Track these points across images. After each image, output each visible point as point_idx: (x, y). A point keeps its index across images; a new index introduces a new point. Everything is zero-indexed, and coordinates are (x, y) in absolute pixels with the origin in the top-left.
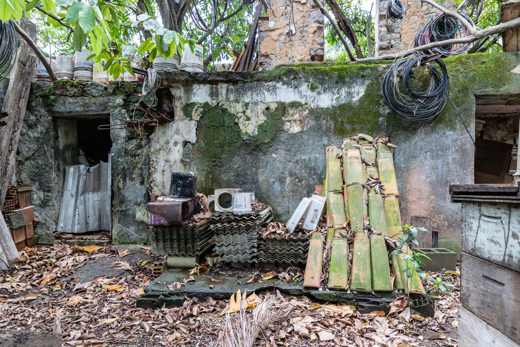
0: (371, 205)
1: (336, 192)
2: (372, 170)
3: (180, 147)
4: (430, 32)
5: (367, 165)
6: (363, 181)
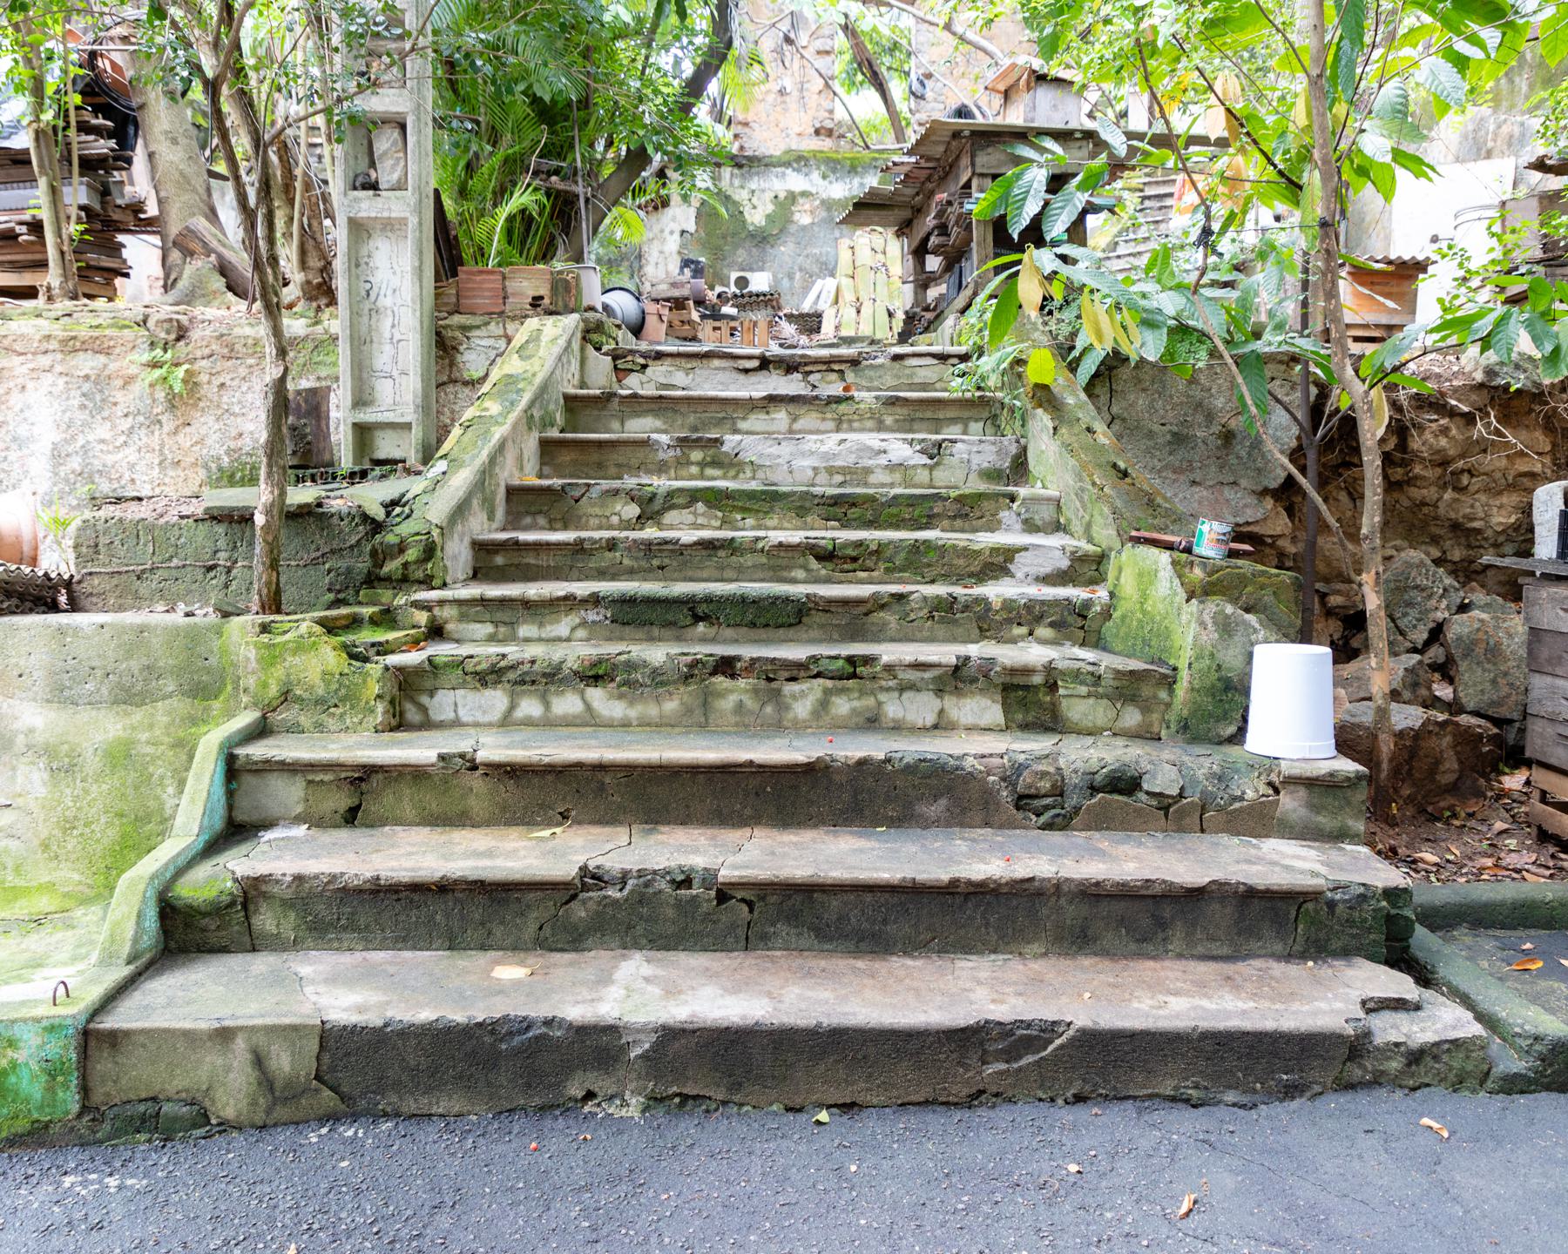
2: (880, 257)
3: (677, 236)
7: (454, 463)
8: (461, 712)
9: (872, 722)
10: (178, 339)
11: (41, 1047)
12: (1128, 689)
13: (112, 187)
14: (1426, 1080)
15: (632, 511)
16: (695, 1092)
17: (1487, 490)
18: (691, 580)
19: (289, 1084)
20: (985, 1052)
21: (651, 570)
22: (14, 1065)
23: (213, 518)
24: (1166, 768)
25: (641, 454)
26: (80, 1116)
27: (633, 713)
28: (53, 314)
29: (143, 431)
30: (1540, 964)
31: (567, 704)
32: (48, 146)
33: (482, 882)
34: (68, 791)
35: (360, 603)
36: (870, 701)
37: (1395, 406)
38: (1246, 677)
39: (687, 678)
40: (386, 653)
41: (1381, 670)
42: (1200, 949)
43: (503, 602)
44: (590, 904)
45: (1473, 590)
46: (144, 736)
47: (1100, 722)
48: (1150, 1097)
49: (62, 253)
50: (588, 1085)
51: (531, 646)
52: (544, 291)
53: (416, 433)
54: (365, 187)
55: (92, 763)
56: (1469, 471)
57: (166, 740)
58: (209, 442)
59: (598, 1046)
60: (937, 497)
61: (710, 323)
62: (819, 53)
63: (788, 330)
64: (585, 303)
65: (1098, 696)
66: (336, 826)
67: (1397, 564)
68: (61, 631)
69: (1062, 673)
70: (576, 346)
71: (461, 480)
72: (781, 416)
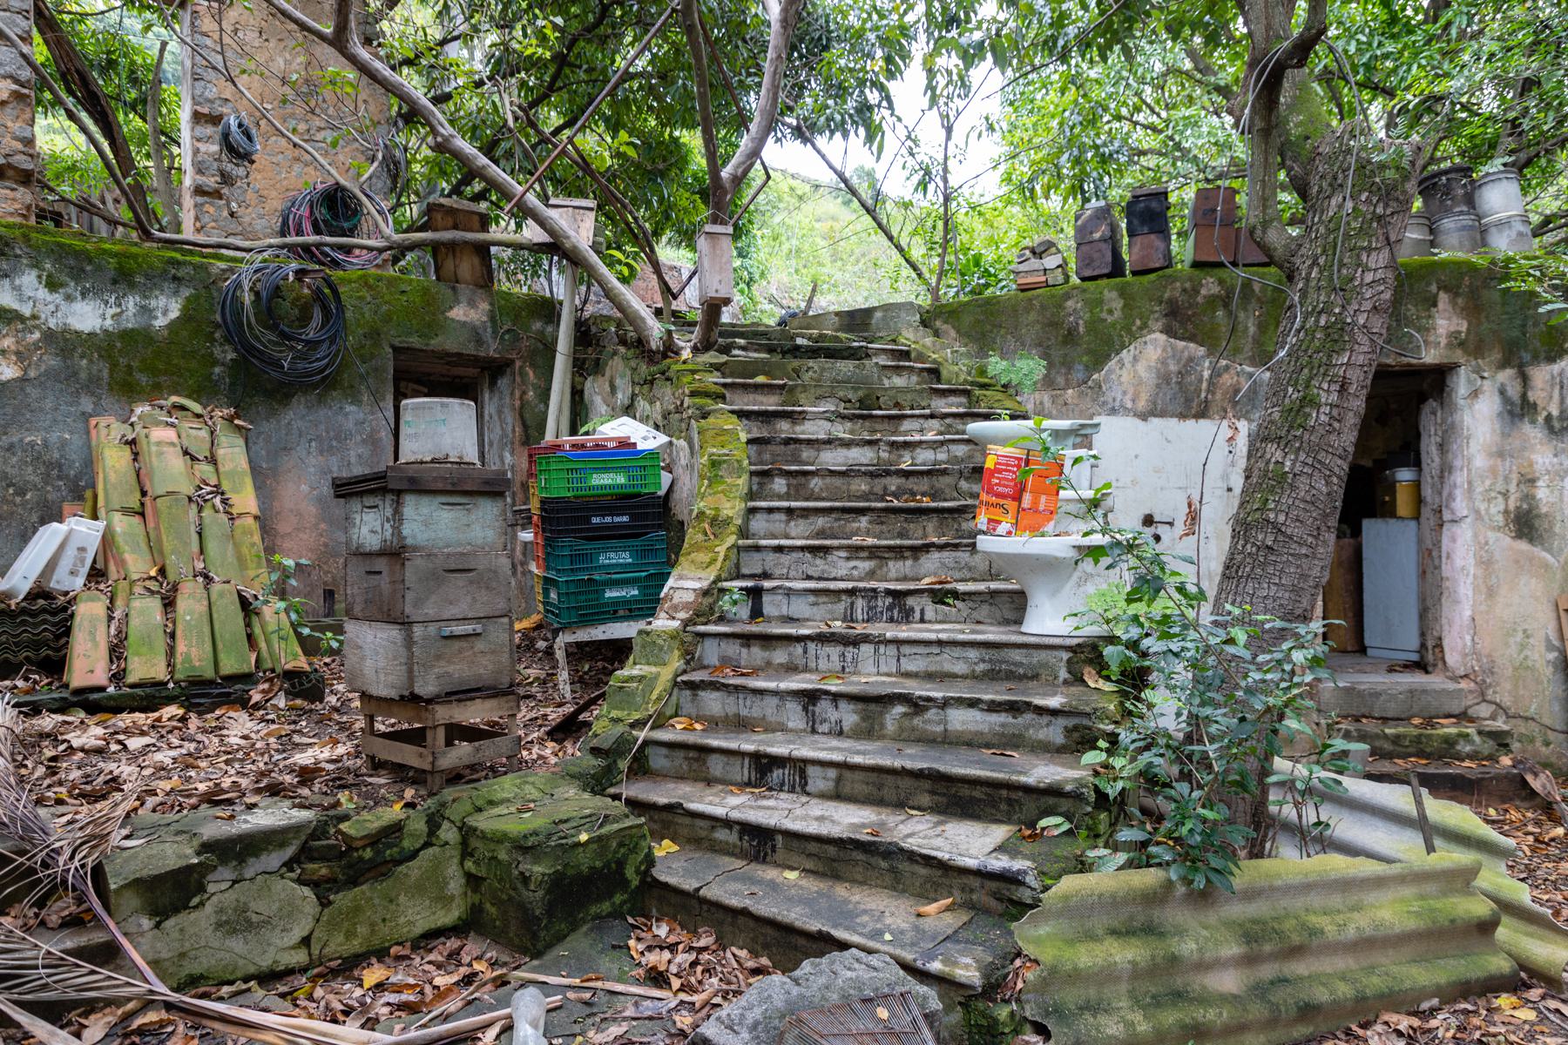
0: (207, 533)
1: (126, 511)
2: (205, 469)
4: (312, 212)
5: (193, 458)
6: (188, 489)
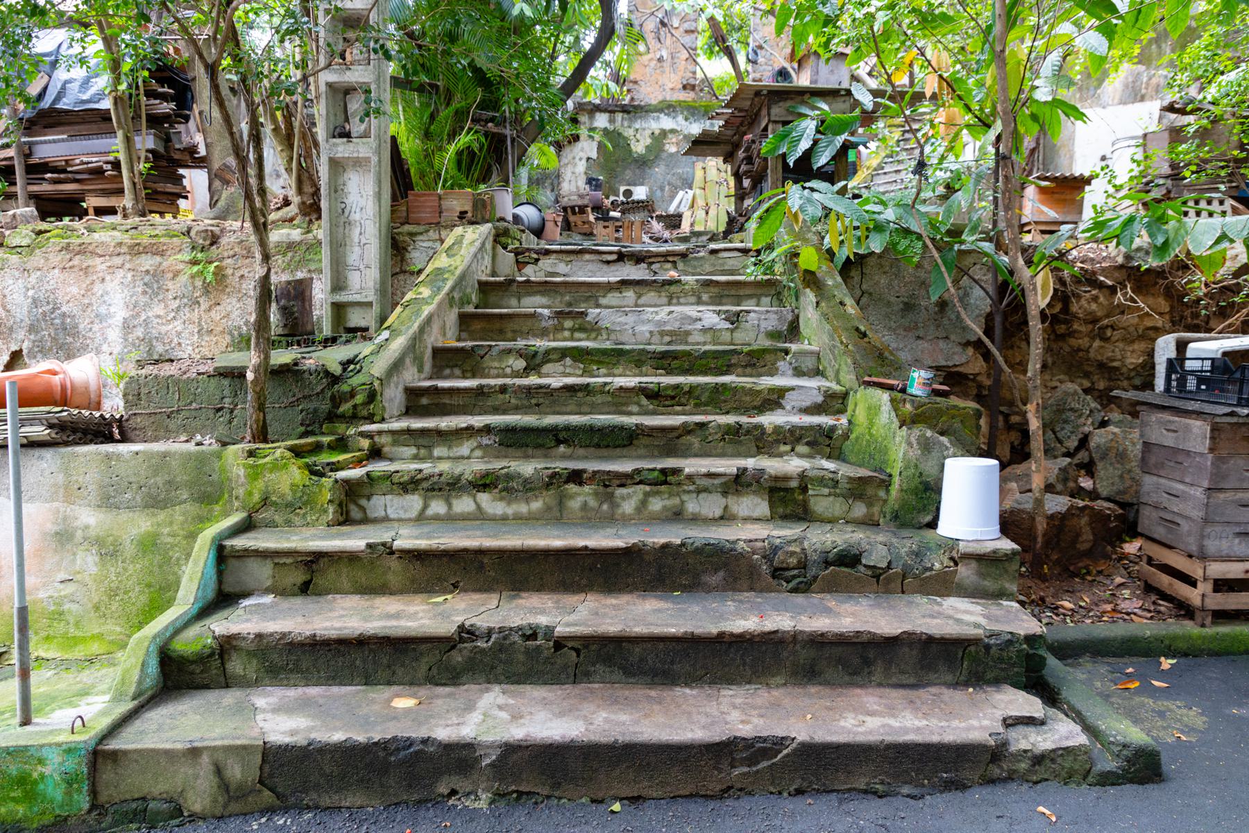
3: (584, 162)
7: (395, 333)
8: (389, 511)
9: (677, 516)
10: (212, 244)
11: (61, 764)
12: (858, 490)
13: (172, 136)
14: (1046, 776)
15: (520, 364)
16: (527, 790)
17: (1124, 340)
18: (558, 413)
19: (240, 787)
20: (733, 759)
21: (530, 407)
22: (42, 776)
23: (221, 374)
24: (878, 547)
25: (529, 323)
26: (89, 811)
27: (510, 511)
28: (124, 228)
29: (187, 309)
30: (1137, 684)
31: (464, 504)
32: (124, 109)
33: (388, 638)
34: (113, 569)
35: (323, 434)
36: (676, 501)
37: (1061, 281)
38: (940, 480)
39: (548, 486)
40: (337, 470)
41: (1040, 470)
42: (894, 680)
43: (424, 432)
44: (465, 652)
45: (1111, 410)
46: (166, 531)
47: (837, 514)
48: (849, 790)
49: (134, 184)
50: (452, 785)
51: (441, 464)
52: (468, 207)
53: (376, 309)
54: (341, 135)
55: (129, 550)
56: (1112, 327)
57: (182, 533)
58: (233, 316)
59: (460, 757)
60: (734, 352)
61: (601, 223)
62: (686, 32)
63: (657, 226)
64: (498, 215)
65: (836, 495)
66: (294, 595)
67: (1059, 393)
68: (108, 457)
69: (811, 479)
70: (489, 246)
71: (398, 344)
72: (630, 294)
